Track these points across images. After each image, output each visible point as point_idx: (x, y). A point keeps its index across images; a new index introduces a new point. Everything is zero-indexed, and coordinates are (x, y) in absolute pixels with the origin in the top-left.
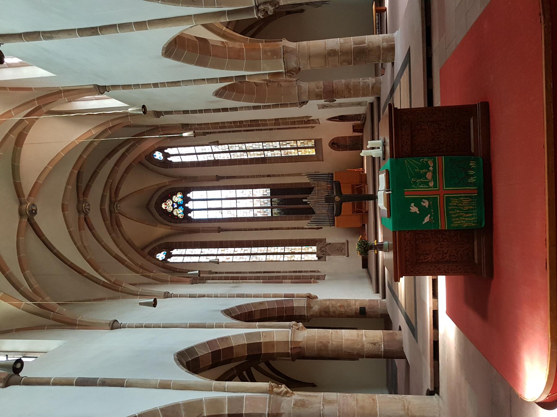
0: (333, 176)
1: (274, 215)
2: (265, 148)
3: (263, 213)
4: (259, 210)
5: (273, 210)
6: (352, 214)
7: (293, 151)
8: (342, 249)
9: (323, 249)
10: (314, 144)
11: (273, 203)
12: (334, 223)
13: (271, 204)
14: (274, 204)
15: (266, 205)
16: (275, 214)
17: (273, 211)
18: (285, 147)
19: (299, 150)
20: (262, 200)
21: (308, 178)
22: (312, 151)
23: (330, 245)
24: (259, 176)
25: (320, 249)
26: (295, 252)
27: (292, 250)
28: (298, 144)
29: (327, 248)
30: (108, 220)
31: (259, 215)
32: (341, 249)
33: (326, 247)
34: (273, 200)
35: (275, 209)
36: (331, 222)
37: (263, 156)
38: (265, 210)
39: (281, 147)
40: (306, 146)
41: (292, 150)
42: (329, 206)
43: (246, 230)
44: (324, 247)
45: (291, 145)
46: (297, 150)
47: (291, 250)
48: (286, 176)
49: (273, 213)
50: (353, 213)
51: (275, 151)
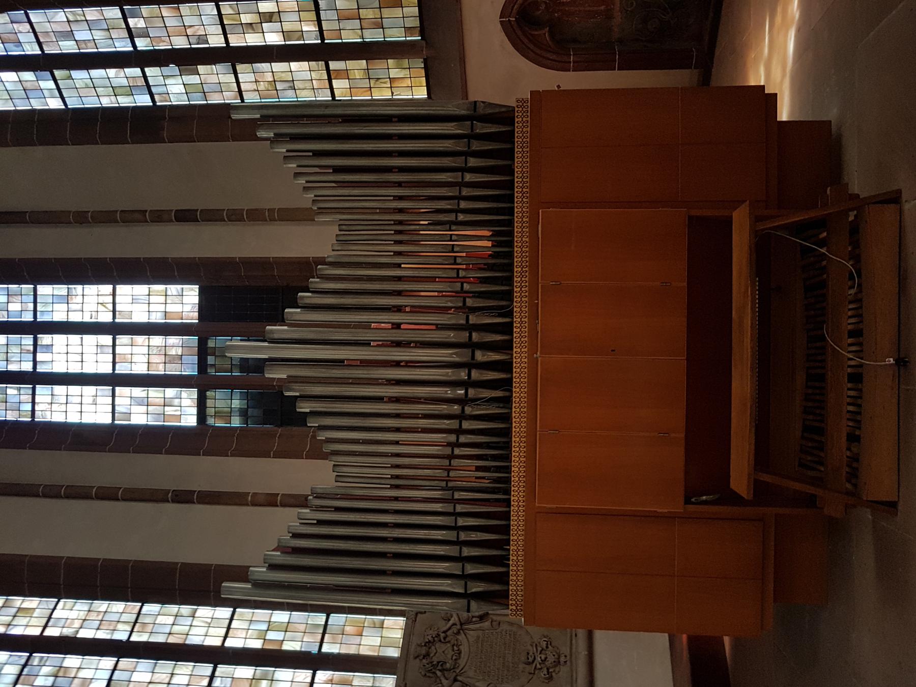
0: (509, 137)
1: (211, 421)
2: (142, 44)
3: (159, 410)
4: (138, 392)
5: (208, 393)
6: (678, 507)
7: (299, 68)
8: (557, 663)
9: (442, 652)
10: (416, 23)
11: (211, 360)
12: (503, 578)
13: (202, 365)
14: (213, 366)
15: (174, 370)
16: (218, 415)
17: (209, 403)
18: (253, 40)
19: (333, 65)
20: (157, 340)
21: (302, 181)
22: (406, 73)
23: (487, 624)
24: (137, 216)
25: (423, 651)
26: (288, 646)
27: (271, 635)
28: (325, 26)
29: (464, 649)
30: (483, 356)
31: (139, 418)
32: (551, 659)
33: (461, 637)
34: (211, 344)
35: (220, 394)
36: (471, 569)
37: (144, 100)
38: (170, 392)
39: (236, 41)
40: (373, 36)
41: (294, 65)
42: (461, 417)
43: (57, 496)
44: (445, 641)
45: (287, 27)
46: (322, 63)
47: (262, 635)
48: (272, 220)
49: (210, 411)
50: (687, 501)
51: (201, 68)
